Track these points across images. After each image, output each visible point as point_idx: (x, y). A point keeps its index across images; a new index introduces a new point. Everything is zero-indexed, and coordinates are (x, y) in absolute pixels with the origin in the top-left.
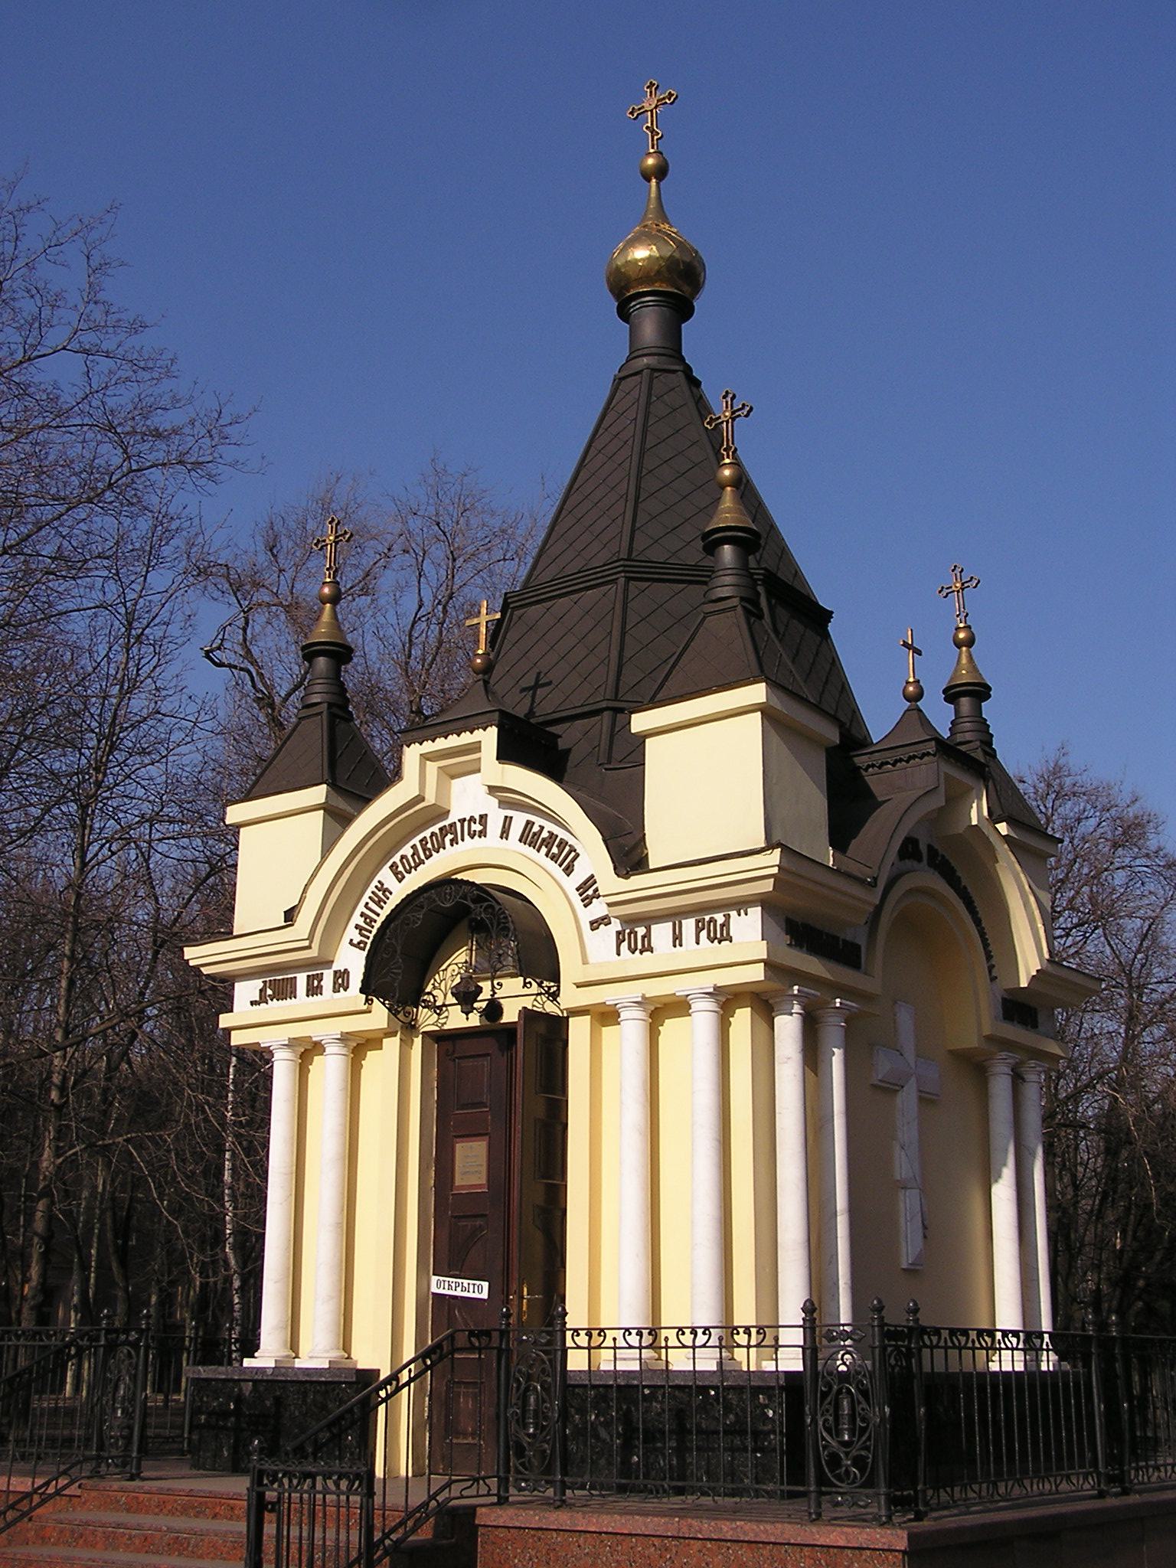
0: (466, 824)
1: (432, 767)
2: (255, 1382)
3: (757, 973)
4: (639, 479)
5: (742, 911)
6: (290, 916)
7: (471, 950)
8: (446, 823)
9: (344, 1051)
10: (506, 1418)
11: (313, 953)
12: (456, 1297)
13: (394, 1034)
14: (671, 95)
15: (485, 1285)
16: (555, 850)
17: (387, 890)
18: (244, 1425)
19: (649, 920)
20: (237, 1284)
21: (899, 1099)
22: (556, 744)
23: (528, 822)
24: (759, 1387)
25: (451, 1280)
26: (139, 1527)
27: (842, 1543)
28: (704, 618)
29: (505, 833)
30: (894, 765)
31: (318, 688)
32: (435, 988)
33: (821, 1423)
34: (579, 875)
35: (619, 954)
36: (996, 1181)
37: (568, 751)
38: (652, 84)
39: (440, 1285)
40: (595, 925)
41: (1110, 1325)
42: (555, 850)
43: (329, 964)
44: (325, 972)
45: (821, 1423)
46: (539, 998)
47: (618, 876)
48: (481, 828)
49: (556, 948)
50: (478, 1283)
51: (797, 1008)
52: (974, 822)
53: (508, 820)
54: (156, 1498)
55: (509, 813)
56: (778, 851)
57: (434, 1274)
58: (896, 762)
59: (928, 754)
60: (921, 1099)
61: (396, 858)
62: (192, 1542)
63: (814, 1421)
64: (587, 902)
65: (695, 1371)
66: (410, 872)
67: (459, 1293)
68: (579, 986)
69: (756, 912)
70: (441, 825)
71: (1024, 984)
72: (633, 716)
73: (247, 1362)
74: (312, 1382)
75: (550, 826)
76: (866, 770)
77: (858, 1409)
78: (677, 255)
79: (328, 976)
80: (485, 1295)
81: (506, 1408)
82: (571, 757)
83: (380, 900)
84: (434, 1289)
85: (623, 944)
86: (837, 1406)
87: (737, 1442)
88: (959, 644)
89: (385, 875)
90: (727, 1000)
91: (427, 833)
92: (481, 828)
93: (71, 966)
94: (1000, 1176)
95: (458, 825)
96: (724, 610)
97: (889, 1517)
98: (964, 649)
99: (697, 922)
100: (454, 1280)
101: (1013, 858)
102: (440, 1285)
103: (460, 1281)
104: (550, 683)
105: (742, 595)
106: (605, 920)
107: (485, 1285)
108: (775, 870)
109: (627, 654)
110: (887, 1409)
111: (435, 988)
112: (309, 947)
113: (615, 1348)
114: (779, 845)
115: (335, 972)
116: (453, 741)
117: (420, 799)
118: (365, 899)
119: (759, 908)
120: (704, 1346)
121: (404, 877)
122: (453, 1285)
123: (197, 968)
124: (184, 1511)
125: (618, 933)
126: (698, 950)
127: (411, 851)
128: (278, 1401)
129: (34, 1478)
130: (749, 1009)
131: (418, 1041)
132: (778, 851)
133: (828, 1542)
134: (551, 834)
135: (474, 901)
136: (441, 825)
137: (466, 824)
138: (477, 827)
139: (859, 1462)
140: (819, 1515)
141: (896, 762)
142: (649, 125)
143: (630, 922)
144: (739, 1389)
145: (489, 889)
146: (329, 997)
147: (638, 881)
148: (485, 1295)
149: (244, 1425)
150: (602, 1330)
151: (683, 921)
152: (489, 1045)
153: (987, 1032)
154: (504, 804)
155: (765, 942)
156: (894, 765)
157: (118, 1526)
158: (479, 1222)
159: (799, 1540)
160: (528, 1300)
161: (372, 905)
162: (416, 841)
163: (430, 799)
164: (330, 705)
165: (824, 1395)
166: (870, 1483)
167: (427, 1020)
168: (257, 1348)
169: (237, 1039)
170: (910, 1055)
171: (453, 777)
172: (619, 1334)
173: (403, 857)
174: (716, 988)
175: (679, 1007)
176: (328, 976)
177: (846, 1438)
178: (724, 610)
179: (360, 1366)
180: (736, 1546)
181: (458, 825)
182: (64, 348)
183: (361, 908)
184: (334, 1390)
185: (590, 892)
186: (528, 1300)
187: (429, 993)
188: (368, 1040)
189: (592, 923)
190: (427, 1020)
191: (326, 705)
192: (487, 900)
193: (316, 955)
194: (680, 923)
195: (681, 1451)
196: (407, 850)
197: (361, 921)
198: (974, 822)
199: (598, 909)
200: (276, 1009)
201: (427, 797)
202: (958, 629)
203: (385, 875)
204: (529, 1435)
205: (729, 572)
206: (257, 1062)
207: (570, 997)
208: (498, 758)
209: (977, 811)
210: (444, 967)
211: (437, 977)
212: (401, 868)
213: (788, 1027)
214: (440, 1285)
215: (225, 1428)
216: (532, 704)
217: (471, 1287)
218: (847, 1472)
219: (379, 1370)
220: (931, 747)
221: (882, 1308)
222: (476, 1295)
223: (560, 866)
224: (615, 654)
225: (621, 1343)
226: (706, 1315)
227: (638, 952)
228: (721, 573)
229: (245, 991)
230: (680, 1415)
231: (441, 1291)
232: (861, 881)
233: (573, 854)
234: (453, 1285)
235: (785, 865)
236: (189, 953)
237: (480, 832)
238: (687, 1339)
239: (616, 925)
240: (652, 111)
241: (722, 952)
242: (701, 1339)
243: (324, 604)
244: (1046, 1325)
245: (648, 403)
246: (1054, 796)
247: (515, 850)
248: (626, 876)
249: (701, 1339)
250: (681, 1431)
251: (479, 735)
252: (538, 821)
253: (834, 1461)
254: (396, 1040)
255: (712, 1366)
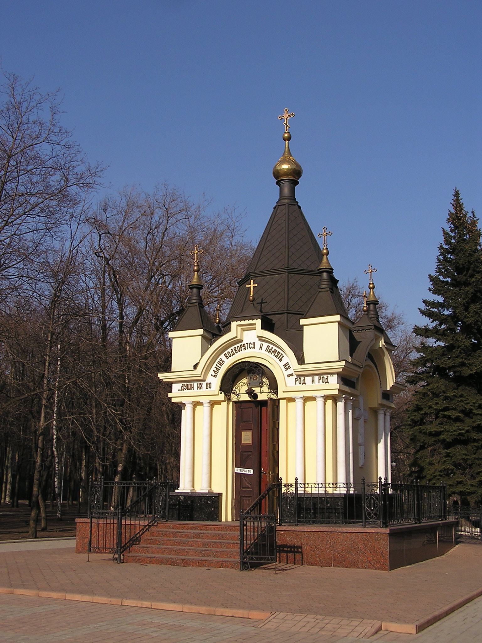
0: (248, 344)
1: (239, 328)
2: (184, 496)
3: (336, 392)
4: (288, 240)
5: (332, 376)
6: (195, 367)
7: (248, 379)
8: (242, 344)
9: (210, 405)
10: (281, 505)
11: (201, 378)
12: (243, 474)
13: (225, 401)
14: (292, 115)
15: (252, 470)
16: (276, 354)
17: (223, 361)
18: (182, 508)
19: (305, 376)
20: (57, 461)
21: (360, 421)
22: (272, 322)
23: (268, 346)
24: (336, 497)
25: (241, 469)
26: (184, 532)
27: (373, 532)
28: (318, 293)
29: (261, 348)
30: (361, 331)
31: (194, 298)
32: (236, 389)
33: (366, 506)
34: (284, 361)
35: (296, 384)
36: (379, 443)
37: (275, 324)
38: (286, 110)
39: (237, 470)
40: (289, 376)
41: (414, 482)
42: (276, 354)
43: (204, 381)
44: (203, 383)
45: (366, 506)
46: (269, 394)
47: (299, 364)
48: (253, 346)
49: (276, 381)
50: (250, 470)
51: (343, 400)
52: (381, 346)
53: (262, 345)
54: (182, 526)
55: (262, 343)
56: (344, 362)
57: (236, 467)
58: (362, 330)
59: (372, 329)
60: (364, 421)
61: (226, 352)
62: (201, 535)
63: (364, 505)
64: (286, 369)
65: (319, 493)
66: (230, 356)
67: (244, 472)
68: (284, 392)
69: (336, 376)
70: (240, 344)
71: (388, 389)
72: (301, 320)
73: (177, 491)
74: (203, 496)
75: (274, 348)
76: (353, 332)
77: (375, 502)
78: (296, 168)
79: (204, 384)
80: (252, 473)
81: (281, 502)
82: (275, 326)
83: (221, 364)
84: (236, 471)
85: (297, 382)
86: (370, 501)
87: (330, 511)
88: (370, 288)
89: (224, 358)
90: (326, 398)
91: (236, 346)
92: (253, 346)
93: (50, 359)
94: (380, 441)
95: (246, 345)
96: (324, 291)
97: (383, 526)
98: (325, 256)
99: (319, 377)
100: (242, 469)
101: (388, 355)
102: (237, 470)
103: (244, 469)
104: (266, 302)
105: (330, 287)
106: (292, 375)
107: (252, 470)
108: (343, 367)
109: (290, 296)
110: (383, 502)
111: (236, 389)
112: (200, 376)
113: (340, 488)
114: (345, 360)
115: (207, 383)
116: (247, 322)
117: (236, 337)
118: (216, 363)
119: (337, 375)
120: (321, 488)
121: (228, 358)
122: (242, 470)
123: (162, 379)
124: (191, 528)
125: (296, 379)
126: (318, 384)
127: (231, 351)
128: (192, 502)
129: (144, 521)
130: (331, 400)
131: (231, 403)
132: (344, 362)
133: (370, 532)
134: (275, 350)
135: (255, 368)
136: (240, 344)
137: (248, 344)
138: (252, 346)
139: (375, 514)
140: (365, 526)
141: (362, 330)
142: (285, 123)
143: (299, 376)
144: (331, 498)
145: (261, 366)
146: (204, 390)
147: (303, 366)
148: (252, 473)
149: (182, 508)
150: (308, 483)
151: (315, 377)
152: (253, 405)
153: (380, 403)
154: (260, 340)
155: (338, 384)
156: (361, 331)
157: (177, 532)
158: (249, 453)
159: (363, 532)
160: (271, 475)
161: (218, 365)
162: (232, 348)
163: (239, 337)
164: (199, 303)
165: (367, 499)
166: (378, 518)
167: (234, 398)
168: (179, 487)
169: (173, 400)
170: (362, 410)
171: (244, 331)
172: (313, 485)
173: (228, 352)
174: (324, 395)
175: (313, 399)
176: (204, 384)
177: (372, 509)
178: (324, 291)
179: (197, 492)
180: (346, 533)
181: (246, 345)
182: (43, 141)
183: (215, 365)
184: (210, 498)
185: (287, 367)
186: (271, 475)
187: (234, 390)
188: (215, 402)
189: (288, 375)
190: (234, 398)
191: (198, 303)
192: (258, 368)
193: (202, 378)
194: (314, 378)
195: (315, 513)
196: (229, 350)
197: (215, 369)
198: (381, 346)
199: (290, 371)
200: (186, 392)
201: (238, 337)
202: (370, 284)
203: (222, 357)
204: (288, 509)
205: (325, 281)
206: (180, 407)
207: (281, 395)
208: (262, 329)
209: (382, 343)
210: (239, 383)
211: (236, 386)
212: (228, 355)
213: (341, 405)
214: (237, 470)
215: (175, 509)
216: (261, 308)
217: (248, 471)
218: (372, 516)
219: (222, 493)
220: (373, 327)
221: (364, 479)
222: (249, 473)
223: (278, 359)
224: (286, 296)
225: (313, 486)
226: (321, 480)
227: (301, 384)
228: (324, 281)
229: (176, 387)
230: (315, 505)
231: (238, 472)
232: (359, 367)
233: (282, 356)
234: (242, 470)
235: (346, 365)
236: (160, 375)
237: (253, 347)
238: (317, 486)
239: (295, 377)
240: (286, 118)
241: (326, 386)
242: (320, 486)
243: (195, 272)
244: (352, 481)
245: (289, 216)
246: (351, 296)
247: (263, 353)
248: (301, 365)
249: (320, 486)
250: (315, 509)
251: (255, 321)
252: (271, 346)
253: (369, 514)
254: (226, 403)
255: (323, 492)
